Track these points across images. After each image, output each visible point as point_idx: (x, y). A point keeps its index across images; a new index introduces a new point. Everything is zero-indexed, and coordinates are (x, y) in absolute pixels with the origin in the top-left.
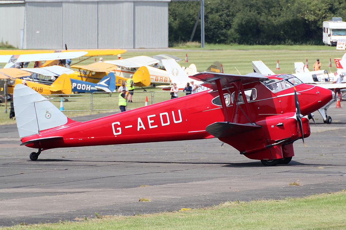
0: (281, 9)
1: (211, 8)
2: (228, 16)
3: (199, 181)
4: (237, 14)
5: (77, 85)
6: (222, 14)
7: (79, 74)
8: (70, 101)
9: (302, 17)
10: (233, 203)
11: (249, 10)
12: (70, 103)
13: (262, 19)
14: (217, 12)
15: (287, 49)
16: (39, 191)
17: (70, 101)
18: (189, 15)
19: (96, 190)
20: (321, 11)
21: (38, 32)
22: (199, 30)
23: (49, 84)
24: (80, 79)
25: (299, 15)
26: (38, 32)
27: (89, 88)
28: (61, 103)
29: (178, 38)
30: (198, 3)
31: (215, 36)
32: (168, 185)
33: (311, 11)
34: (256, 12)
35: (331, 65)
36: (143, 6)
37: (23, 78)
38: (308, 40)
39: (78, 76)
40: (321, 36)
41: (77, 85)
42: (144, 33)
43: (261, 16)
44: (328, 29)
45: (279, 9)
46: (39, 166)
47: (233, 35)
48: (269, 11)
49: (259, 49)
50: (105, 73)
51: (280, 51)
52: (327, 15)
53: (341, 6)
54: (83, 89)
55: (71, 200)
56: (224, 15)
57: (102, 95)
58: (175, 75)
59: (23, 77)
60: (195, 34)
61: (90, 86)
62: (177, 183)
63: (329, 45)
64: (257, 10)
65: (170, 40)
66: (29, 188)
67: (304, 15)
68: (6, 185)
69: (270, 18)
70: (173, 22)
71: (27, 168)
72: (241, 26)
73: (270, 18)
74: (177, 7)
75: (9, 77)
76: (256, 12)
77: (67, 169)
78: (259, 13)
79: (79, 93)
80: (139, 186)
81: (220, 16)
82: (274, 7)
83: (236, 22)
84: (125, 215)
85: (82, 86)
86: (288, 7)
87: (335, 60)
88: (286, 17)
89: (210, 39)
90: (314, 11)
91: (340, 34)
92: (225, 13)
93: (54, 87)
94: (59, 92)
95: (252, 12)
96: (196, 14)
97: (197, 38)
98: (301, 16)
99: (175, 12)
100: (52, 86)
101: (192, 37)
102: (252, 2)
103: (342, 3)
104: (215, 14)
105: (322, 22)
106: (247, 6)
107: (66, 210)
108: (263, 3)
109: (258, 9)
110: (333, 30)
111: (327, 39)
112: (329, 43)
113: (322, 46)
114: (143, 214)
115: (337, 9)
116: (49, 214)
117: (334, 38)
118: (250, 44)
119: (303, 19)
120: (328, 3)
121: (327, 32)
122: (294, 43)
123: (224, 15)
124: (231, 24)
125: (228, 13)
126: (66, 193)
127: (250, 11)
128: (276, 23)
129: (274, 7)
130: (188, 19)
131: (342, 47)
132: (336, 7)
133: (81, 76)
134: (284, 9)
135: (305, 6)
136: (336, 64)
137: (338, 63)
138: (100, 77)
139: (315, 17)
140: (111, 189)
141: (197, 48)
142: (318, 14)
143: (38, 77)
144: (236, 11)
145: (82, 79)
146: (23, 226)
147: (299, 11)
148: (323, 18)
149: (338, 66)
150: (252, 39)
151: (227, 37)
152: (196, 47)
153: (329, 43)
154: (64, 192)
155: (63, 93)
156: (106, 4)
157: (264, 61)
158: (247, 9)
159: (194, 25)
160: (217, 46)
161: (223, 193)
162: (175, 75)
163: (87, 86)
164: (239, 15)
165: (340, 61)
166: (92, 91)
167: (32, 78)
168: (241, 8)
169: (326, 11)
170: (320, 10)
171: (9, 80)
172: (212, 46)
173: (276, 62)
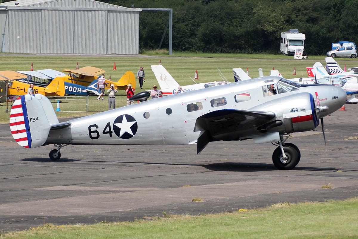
0: (242, 21)
1: (178, 18)
2: (193, 25)
3: (234, 182)
4: (202, 24)
5: (68, 88)
6: (188, 24)
7: (69, 77)
8: (63, 103)
9: (262, 29)
10: (284, 205)
11: (212, 20)
12: (63, 103)
13: (225, 29)
14: (184, 22)
15: (248, 58)
16: (91, 190)
17: (63, 103)
18: (158, 24)
19: (144, 189)
20: (279, 23)
21: (18, 37)
22: (167, 38)
23: (45, 86)
24: (70, 82)
25: (259, 27)
26: (18, 37)
27: (80, 90)
28: (58, 104)
29: (147, 45)
30: (166, 13)
31: (181, 44)
32: (208, 185)
33: (270, 22)
34: (220, 22)
35: (295, 73)
36: (22, 12)
37: (19, 80)
38: (267, 49)
39: (68, 79)
40: (279, 47)
41: (68, 88)
42: (49, 38)
43: (224, 26)
44: (286, 40)
45: (240, 20)
46: (76, 165)
47: (198, 44)
48: (232, 22)
49: (223, 57)
50: (93, 77)
51: (242, 60)
52: (285, 26)
53: (297, 18)
54: (74, 91)
55: (129, 199)
56: (190, 25)
57: (91, 97)
58: (163, 80)
59: (19, 79)
60: (163, 42)
61: (81, 89)
62: (214, 184)
63: (287, 55)
64: (221, 21)
65: (140, 47)
66: (79, 186)
67: (264, 26)
68: (54, 182)
69: (232, 28)
70: (143, 30)
71: (66, 167)
72: (205, 35)
73: (232, 28)
74: (146, 17)
75: (7, 78)
76: (220, 22)
77: (104, 169)
78: (222, 24)
79: (69, 95)
80: (182, 186)
81: (186, 25)
82: (236, 18)
83: (200, 31)
84: (191, 215)
85: (73, 89)
86: (249, 18)
87: (307, 68)
88: (247, 28)
89: (177, 47)
90: (272, 22)
91: (296, 45)
92: (190, 23)
93: (49, 89)
94: (54, 94)
95: (216, 23)
96: (164, 23)
97: (165, 46)
98: (261, 27)
99: (145, 21)
100: (47, 88)
101: (161, 44)
102: (216, 13)
103: (299, 16)
104: (182, 24)
105: (280, 33)
106: (211, 16)
107: (129, 209)
108: (225, 14)
109: (221, 20)
110: (291, 41)
111: (284, 49)
112: (286, 53)
113: (280, 55)
114: (207, 214)
115: (294, 21)
116: (115, 212)
117: (291, 48)
118: (214, 52)
119: (263, 30)
120: (285, 16)
121: (285, 43)
122: (254, 52)
123: (190, 25)
124: (196, 33)
125: (194, 23)
126: (119, 192)
127: (214, 22)
128: (238, 33)
129: (236, 18)
130: (157, 28)
131: (299, 57)
132: (293, 19)
133: (71, 79)
134: (245, 20)
135: (265, 18)
136: (308, 72)
137: (310, 71)
138: (89, 80)
139: (274, 29)
140: (158, 189)
141: (165, 55)
142: (277, 26)
143: (33, 79)
144: (201, 21)
145: (72, 81)
146: (104, 224)
147: (259, 22)
148: (280, 29)
149: (310, 74)
150: (215, 47)
151: (192, 45)
152: (164, 54)
153: (286, 53)
154: (116, 191)
155: (57, 95)
156: (20, 11)
157: (242, 68)
158: (212, 20)
159: (162, 33)
160: (183, 54)
161: (265, 195)
162: (163, 80)
163: (78, 88)
164: (203, 25)
165: (311, 70)
166: (82, 94)
167: (27, 81)
168: (205, 18)
169: (283, 23)
170: (278, 22)
171: (7, 81)
172: (179, 54)
173: (247, 69)
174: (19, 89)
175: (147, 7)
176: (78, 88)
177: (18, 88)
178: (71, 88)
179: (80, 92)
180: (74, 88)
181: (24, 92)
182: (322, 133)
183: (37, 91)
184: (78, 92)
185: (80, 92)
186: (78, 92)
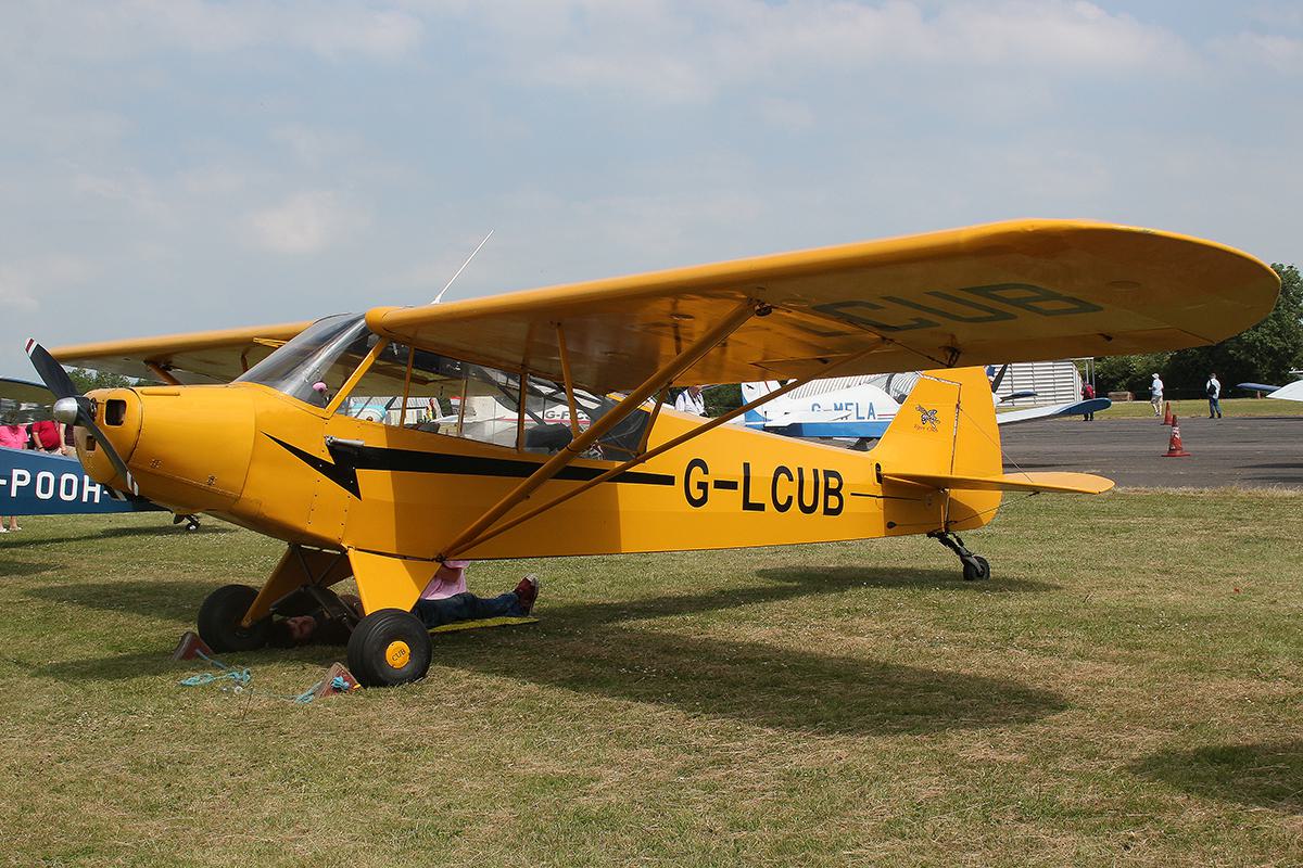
5: (34, 480)
41: (34, 480)
85: (58, 482)
174: (703, 486)
175: (1265, 370)
176: (87, 478)
177: (697, 475)
178: (46, 481)
179: (97, 500)
180: (65, 477)
181: (748, 506)
182: (516, 416)
183: (836, 492)
184: (85, 499)
185: (97, 500)
186: (85, 499)
